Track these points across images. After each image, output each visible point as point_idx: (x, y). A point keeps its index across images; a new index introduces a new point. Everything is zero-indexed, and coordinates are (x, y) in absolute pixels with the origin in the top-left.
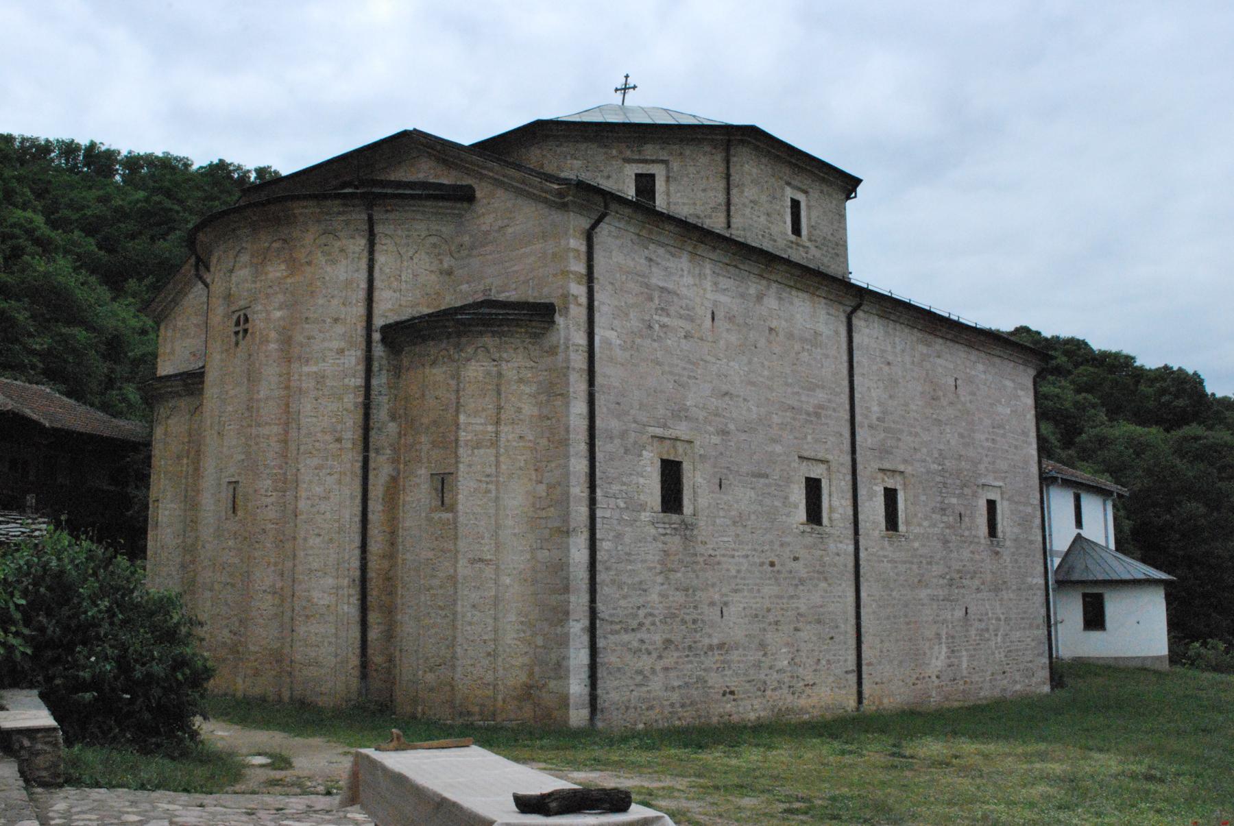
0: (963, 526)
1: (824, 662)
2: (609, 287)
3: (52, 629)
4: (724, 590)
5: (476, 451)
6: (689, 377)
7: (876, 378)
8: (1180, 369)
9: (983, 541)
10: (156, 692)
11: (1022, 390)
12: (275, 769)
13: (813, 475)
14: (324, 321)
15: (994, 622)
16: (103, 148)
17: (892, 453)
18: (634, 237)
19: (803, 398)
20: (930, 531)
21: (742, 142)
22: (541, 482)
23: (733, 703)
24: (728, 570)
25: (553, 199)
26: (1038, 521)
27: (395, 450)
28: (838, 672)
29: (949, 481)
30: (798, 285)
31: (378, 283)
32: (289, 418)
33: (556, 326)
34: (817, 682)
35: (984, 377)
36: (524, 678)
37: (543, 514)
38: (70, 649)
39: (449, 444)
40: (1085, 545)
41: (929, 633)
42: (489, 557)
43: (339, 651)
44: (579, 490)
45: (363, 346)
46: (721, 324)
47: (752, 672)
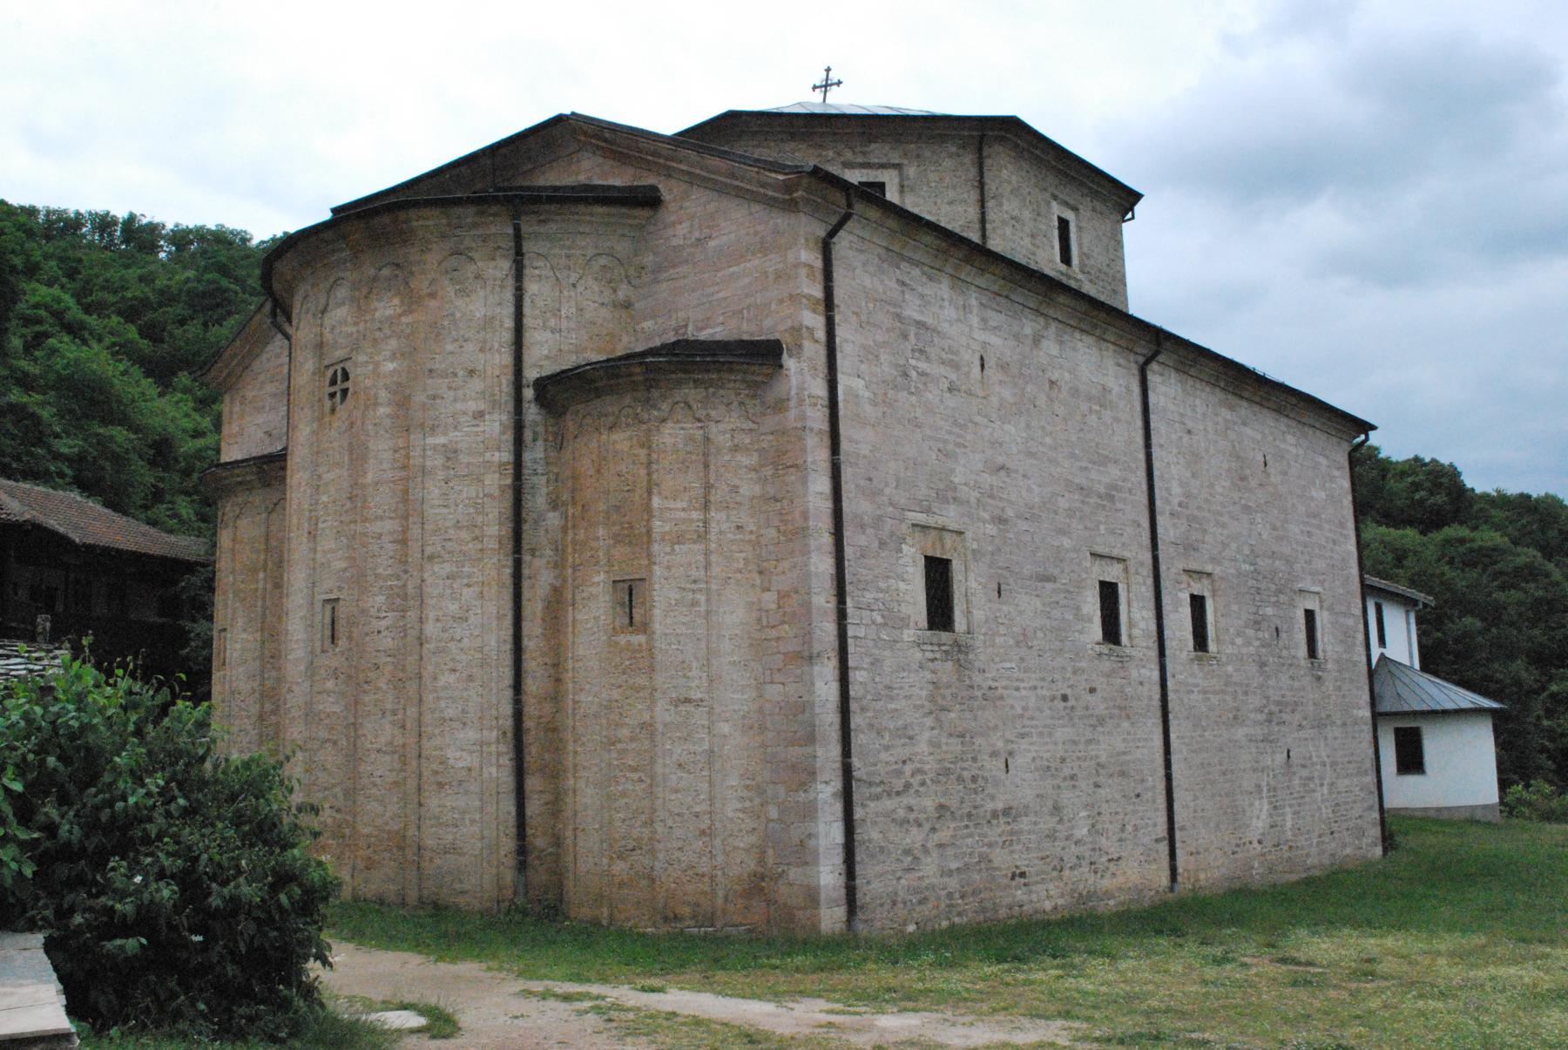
0: (1281, 643)
3: (68, 830)
4: (1008, 735)
5: (676, 547)
8: (1434, 461)
10: (246, 926)
11: (1338, 469)
12: (434, 1037)
13: (1108, 579)
14: (455, 375)
16: (145, 221)
18: (882, 251)
19: (1093, 475)
20: (1244, 650)
21: (1002, 140)
23: (1024, 889)
24: (1012, 707)
27: (559, 550)
28: (1146, 840)
29: (1263, 586)
31: (527, 321)
32: (408, 507)
35: (1294, 451)
36: (752, 865)
37: (774, 633)
38: (99, 862)
39: (636, 536)
40: (1393, 669)
41: (1248, 784)
42: (699, 696)
43: (486, 833)
44: (824, 600)
45: (511, 407)
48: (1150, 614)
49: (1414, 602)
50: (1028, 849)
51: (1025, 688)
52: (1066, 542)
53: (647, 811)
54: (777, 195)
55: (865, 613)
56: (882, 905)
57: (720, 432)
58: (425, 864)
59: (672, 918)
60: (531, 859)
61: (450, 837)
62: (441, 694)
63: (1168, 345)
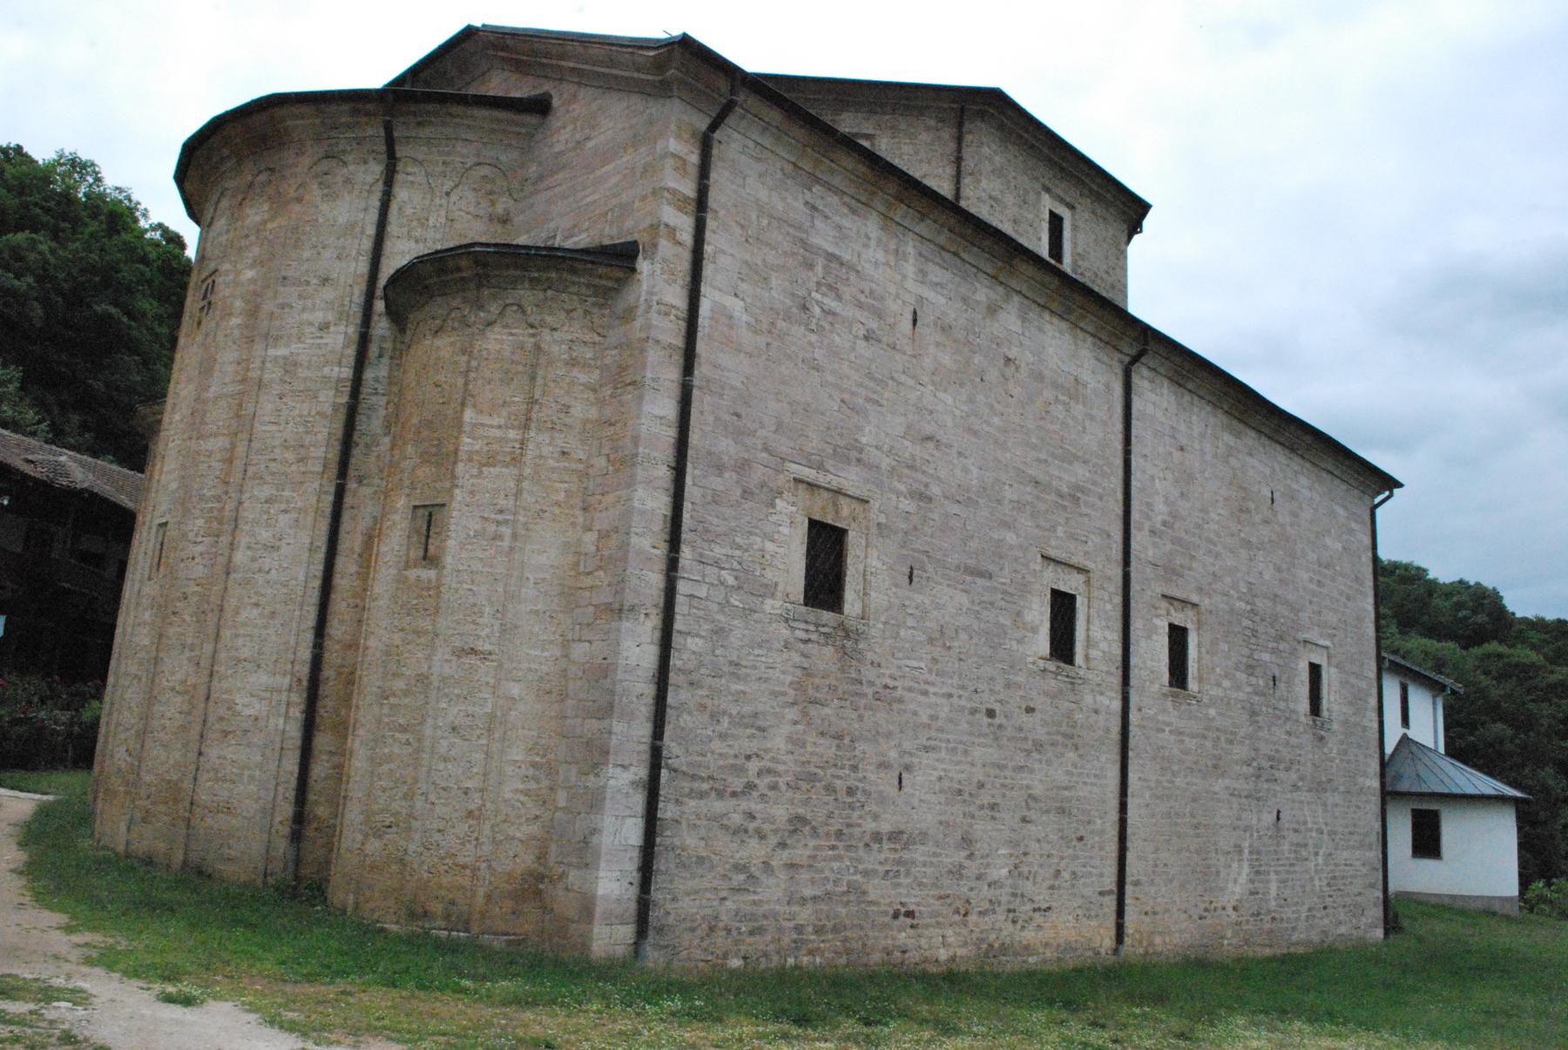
0: (1278, 693)
1: (1066, 875)
2: (738, 230)
4: (907, 745)
6: (868, 400)
7: (1162, 465)
8: (1478, 584)
9: (1303, 719)
13: (1063, 588)
14: (308, 283)
15: (1314, 834)
17: (1182, 576)
18: (789, 168)
21: (982, 115)
22: (590, 530)
23: (909, 931)
24: (915, 714)
25: (650, 77)
26: (1373, 702)
28: (1088, 892)
30: (1054, 306)
31: (393, 228)
32: (243, 424)
33: (638, 276)
34: (1054, 904)
36: (527, 860)
37: (588, 581)
39: (443, 457)
40: (1414, 748)
42: (487, 647)
44: (648, 542)
46: (926, 330)
47: (946, 881)
48: (1115, 636)
49: (1443, 687)
50: (920, 884)
51: (934, 694)
52: (1011, 538)
53: (409, 781)
54: (650, 77)
55: (709, 570)
56: (693, 930)
57: (555, 341)
58: (195, 822)
59: (416, 913)
60: (309, 832)
61: (226, 793)
62: (242, 631)
63: (1152, 346)
